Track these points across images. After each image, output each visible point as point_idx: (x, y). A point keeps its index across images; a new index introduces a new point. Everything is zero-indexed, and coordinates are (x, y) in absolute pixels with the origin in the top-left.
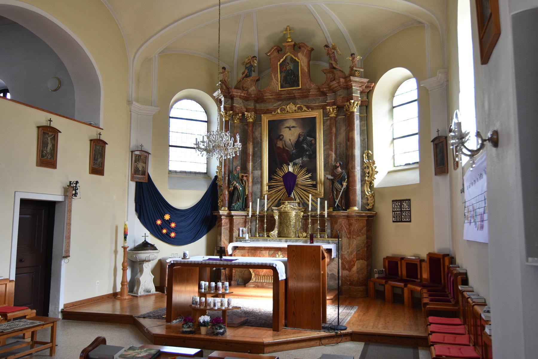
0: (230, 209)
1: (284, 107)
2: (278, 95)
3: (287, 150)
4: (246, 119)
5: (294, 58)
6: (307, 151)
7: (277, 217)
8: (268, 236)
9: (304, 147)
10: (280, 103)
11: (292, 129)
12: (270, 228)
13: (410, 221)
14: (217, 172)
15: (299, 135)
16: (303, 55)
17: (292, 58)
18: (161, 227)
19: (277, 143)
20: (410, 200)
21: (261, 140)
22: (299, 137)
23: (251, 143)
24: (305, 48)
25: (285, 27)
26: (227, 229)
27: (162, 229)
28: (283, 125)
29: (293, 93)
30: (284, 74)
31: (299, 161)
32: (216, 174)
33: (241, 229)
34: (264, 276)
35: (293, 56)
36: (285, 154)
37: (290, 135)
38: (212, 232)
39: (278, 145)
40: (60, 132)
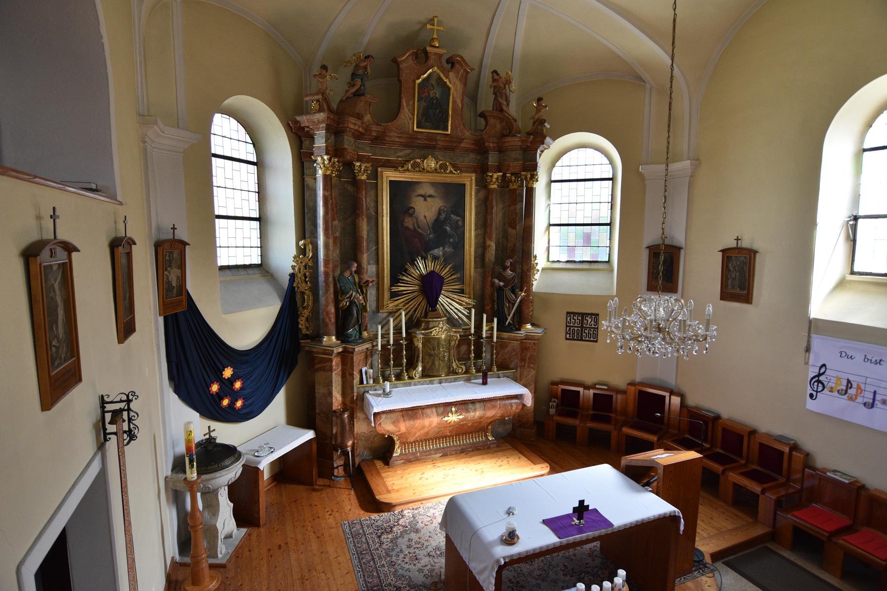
0: (342, 336)
2: (411, 138)
4: (354, 177)
6: (450, 236)
7: (420, 345)
8: (411, 378)
10: (408, 151)
11: (428, 199)
12: (411, 365)
13: (596, 341)
15: (440, 210)
16: (457, 77)
17: (440, 79)
18: (220, 397)
19: (403, 221)
20: (598, 315)
21: (377, 213)
22: (439, 214)
23: (365, 220)
24: (462, 66)
25: (430, 17)
27: (222, 399)
29: (436, 140)
30: (424, 104)
31: (439, 252)
32: (291, 271)
33: (364, 370)
34: (414, 442)
35: (442, 75)
36: (416, 240)
37: (426, 210)
39: (406, 225)
40: (77, 250)
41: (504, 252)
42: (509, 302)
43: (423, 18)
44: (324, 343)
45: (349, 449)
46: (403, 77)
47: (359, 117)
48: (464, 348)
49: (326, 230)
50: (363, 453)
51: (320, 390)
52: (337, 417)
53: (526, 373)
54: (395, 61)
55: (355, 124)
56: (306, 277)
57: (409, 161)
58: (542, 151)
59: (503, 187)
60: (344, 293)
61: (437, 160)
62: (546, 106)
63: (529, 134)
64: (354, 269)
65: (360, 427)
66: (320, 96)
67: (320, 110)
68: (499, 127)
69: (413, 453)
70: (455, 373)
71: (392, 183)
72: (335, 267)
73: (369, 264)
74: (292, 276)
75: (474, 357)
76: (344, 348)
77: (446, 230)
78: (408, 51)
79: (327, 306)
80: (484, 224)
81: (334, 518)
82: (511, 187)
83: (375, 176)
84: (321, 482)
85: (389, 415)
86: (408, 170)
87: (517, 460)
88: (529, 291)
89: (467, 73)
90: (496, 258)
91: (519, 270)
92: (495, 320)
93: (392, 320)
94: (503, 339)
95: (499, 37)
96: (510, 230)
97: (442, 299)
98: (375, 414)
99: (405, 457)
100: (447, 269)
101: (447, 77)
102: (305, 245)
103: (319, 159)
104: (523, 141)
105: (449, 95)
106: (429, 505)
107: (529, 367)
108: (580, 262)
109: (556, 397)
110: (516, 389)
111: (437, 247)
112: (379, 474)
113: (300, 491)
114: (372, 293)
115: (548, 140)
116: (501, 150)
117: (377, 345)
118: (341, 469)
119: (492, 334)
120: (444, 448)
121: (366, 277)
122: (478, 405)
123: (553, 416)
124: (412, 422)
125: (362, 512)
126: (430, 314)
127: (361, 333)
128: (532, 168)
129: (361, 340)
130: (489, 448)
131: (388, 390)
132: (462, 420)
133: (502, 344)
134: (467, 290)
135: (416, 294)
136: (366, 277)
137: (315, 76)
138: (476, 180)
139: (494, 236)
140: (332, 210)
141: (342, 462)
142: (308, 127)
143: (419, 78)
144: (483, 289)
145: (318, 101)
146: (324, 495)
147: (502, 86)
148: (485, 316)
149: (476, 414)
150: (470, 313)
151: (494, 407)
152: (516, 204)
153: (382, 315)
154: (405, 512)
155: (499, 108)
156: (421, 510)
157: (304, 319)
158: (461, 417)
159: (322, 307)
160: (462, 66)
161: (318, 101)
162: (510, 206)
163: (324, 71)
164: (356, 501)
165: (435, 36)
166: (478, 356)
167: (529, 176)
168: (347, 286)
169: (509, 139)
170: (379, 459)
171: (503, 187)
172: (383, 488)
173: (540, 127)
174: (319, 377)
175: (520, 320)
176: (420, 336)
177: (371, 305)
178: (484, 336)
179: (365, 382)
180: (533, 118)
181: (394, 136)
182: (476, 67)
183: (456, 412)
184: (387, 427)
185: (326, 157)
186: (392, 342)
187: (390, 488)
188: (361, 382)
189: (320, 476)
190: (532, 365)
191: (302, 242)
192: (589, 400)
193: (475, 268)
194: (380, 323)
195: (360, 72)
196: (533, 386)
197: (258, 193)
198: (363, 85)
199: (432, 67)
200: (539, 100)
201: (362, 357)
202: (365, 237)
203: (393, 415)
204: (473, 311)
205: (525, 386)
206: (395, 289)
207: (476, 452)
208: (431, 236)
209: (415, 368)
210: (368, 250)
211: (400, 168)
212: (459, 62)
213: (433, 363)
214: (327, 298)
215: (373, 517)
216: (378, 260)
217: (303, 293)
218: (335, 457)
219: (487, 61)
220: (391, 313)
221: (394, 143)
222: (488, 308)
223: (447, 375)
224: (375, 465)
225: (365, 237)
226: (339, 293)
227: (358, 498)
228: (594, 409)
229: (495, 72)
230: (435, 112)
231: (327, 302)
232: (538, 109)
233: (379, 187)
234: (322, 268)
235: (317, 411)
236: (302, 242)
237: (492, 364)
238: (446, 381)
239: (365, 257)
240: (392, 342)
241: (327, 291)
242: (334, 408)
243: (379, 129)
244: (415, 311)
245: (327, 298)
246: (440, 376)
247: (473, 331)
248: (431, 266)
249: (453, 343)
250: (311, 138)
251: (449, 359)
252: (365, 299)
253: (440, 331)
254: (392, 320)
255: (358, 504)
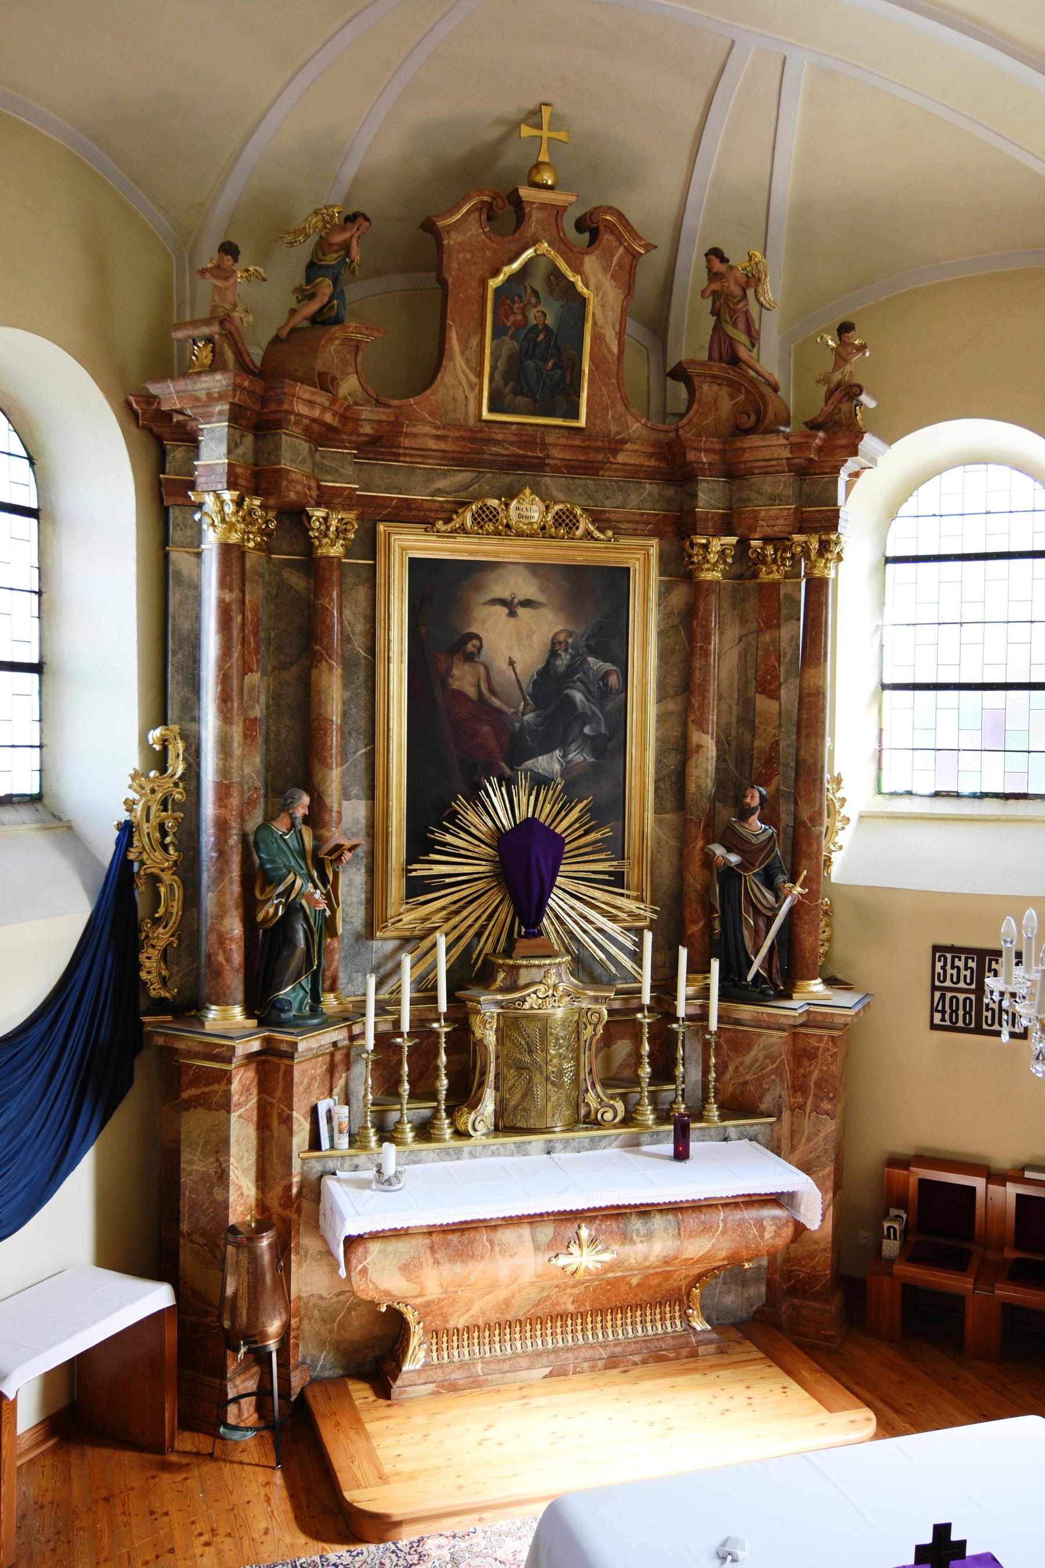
0: (261, 1005)
1: (494, 503)
2: (473, 440)
3: (498, 711)
4: (309, 548)
5: (571, 277)
6: (585, 719)
7: (490, 1038)
8: (461, 1134)
9: (570, 701)
10: (464, 476)
11: (521, 611)
12: (463, 1095)
14: (130, 805)
15: (554, 643)
16: (606, 270)
17: (555, 273)
19: (449, 670)
21: (372, 650)
22: (553, 654)
23: (338, 671)
24: (620, 239)
25: (531, 105)
26: (248, 1120)
28: (478, 587)
29: (544, 446)
30: (510, 345)
31: (549, 763)
32: (124, 816)
36: (486, 729)
37: (514, 642)
38: (123, 1121)
39: (455, 685)
41: (742, 766)
42: (757, 913)
43: (509, 109)
44: (209, 1027)
45: (272, 1345)
46: (453, 269)
47: (325, 383)
48: (622, 1048)
49: (224, 699)
50: (314, 1358)
51: (193, 1165)
52: (238, 1246)
53: (807, 1126)
54: (428, 226)
55: (311, 403)
56: (164, 833)
57: (465, 504)
58: (856, 475)
59: (740, 577)
60: (270, 880)
61: (547, 500)
62: (862, 348)
63: (814, 426)
64: (301, 811)
65: (308, 1280)
66: (216, 328)
67: (216, 366)
68: (726, 405)
69: (462, 1365)
70: (593, 1122)
71: (416, 566)
72: (248, 805)
73: (346, 795)
74: (127, 830)
75: (654, 1076)
76: (267, 1040)
77: (572, 701)
78: (465, 199)
79: (220, 917)
80: (683, 682)
81: (219, 1553)
82: (764, 576)
83: (368, 545)
84: (187, 1442)
85: (393, 1245)
86: (463, 530)
87: (778, 1395)
88: (814, 883)
89: (635, 256)
90: (720, 782)
91: (786, 819)
92: (715, 965)
93: (407, 960)
94: (738, 1022)
95: (728, 156)
96: (762, 702)
97: (556, 901)
98: (351, 1242)
99: (439, 1375)
100: (575, 814)
101: (578, 270)
102: (164, 742)
103: (209, 500)
104: (795, 447)
105: (583, 319)
106: (503, 1525)
107: (816, 1109)
108: (974, 796)
109: (902, 1204)
110: (778, 1175)
111: (548, 750)
112: (358, 1423)
113: (124, 1467)
114: (351, 881)
115: (869, 442)
116: (733, 473)
117: (362, 1035)
118: (248, 1405)
119: (705, 1008)
120: (555, 1351)
121: (335, 836)
122: (658, 1222)
123: (891, 1262)
124: (458, 1268)
125: (302, 1539)
126: (522, 945)
127: (316, 999)
128: (822, 521)
129: (315, 1017)
130: (694, 1354)
131: (390, 1170)
132: (610, 1267)
133: (735, 1039)
134: (632, 876)
135: (481, 885)
136: (335, 836)
137: (203, 272)
138: (661, 558)
139: (713, 717)
140: (244, 642)
141: (251, 1385)
142: (180, 412)
143: (496, 273)
144: (680, 873)
145: (209, 340)
146: (193, 1484)
147: (736, 291)
148: (683, 953)
149: (653, 1248)
150: (640, 944)
151: (707, 1229)
152: (778, 627)
153: (383, 945)
154: (430, 1545)
155: (727, 355)
156: (478, 1541)
157: (155, 953)
158: (607, 1257)
159: (207, 922)
160: (620, 239)
161: (209, 340)
162: (759, 631)
163: (228, 260)
164: (287, 1506)
165: (544, 157)
166: (664, 1072)
167: (815, 545)
168: (280, 861)
169: (754, 440)
170: (360, 1376)
171: (740, 577)
172: (367, 1468)
173: (845, 407)
174: (194, 1124)
175: (790, 965)
176: (488, 1006)
177: (351, 913)
178: (681, 1013)
179: (325, 1143)
180: (826, 380)
181: (423, 433)
182: (663, 241)
183: (593, 1241)
184: (384, 1278)
185: (228, 496)
186: (406, 1027)
187: (387, 1469)
188: (315, 1144)
189: (187, 1423)
190: (826, 1105)
191: (155, 734)
192: (1002, 1218)
193: (659, 810)
194: (375, 970)
195: (331, 259)
196: (830, 1169)
197: (40, 593)
198: (338, 294)
199: (534, 242)
200: (845, 329)
201: (320, 1068)
202: (336, 719)
203: (402, 1246)
204: (648, 936)
205: (806, 1168)
206: (421, 870)
207: (653, 1367)
208: (529, 717)
209: (474, 1104)
210: (344, 754)
211: (440, 525)
212: (611, 228)
213: (528, 1093)
214: (221, 894)
215: (332, 1557)
216: (372, 787)
217: (154, 879)
218: (231, 1368)
219: (695, 221)
220: (406, 942)
221: (424, 453)
222: (694, 929)
223: (571, 1127)
224: (347, 1395)
225: (336, 719)
226: (256, 879)
227: (292, 1497)
228: (1018, 1245)
229: (715, 253)
230: (542, 369)
231: (221, 905)
232: (841, 357)
233: (380, 579)
234: (209, 809)
235: (185, 1227)
236: (155, 734)
237: (705, 1099)
238: (566, 1145)
239: (334, 779)
240: (406, 1027)
241: (221, 873)
242: (233, 1220)
243: (382, 414)
244: (479, 934)
245: (221, 894)
246: (548, 1130)
247: (646, 998)
248: (525, 808)
249: (587, 1033)
250: (191, 440)
251: (576, 1080)
252: (332, 899)
253: (552, 994)
254: (407, 960)
255: (291, 1515)
